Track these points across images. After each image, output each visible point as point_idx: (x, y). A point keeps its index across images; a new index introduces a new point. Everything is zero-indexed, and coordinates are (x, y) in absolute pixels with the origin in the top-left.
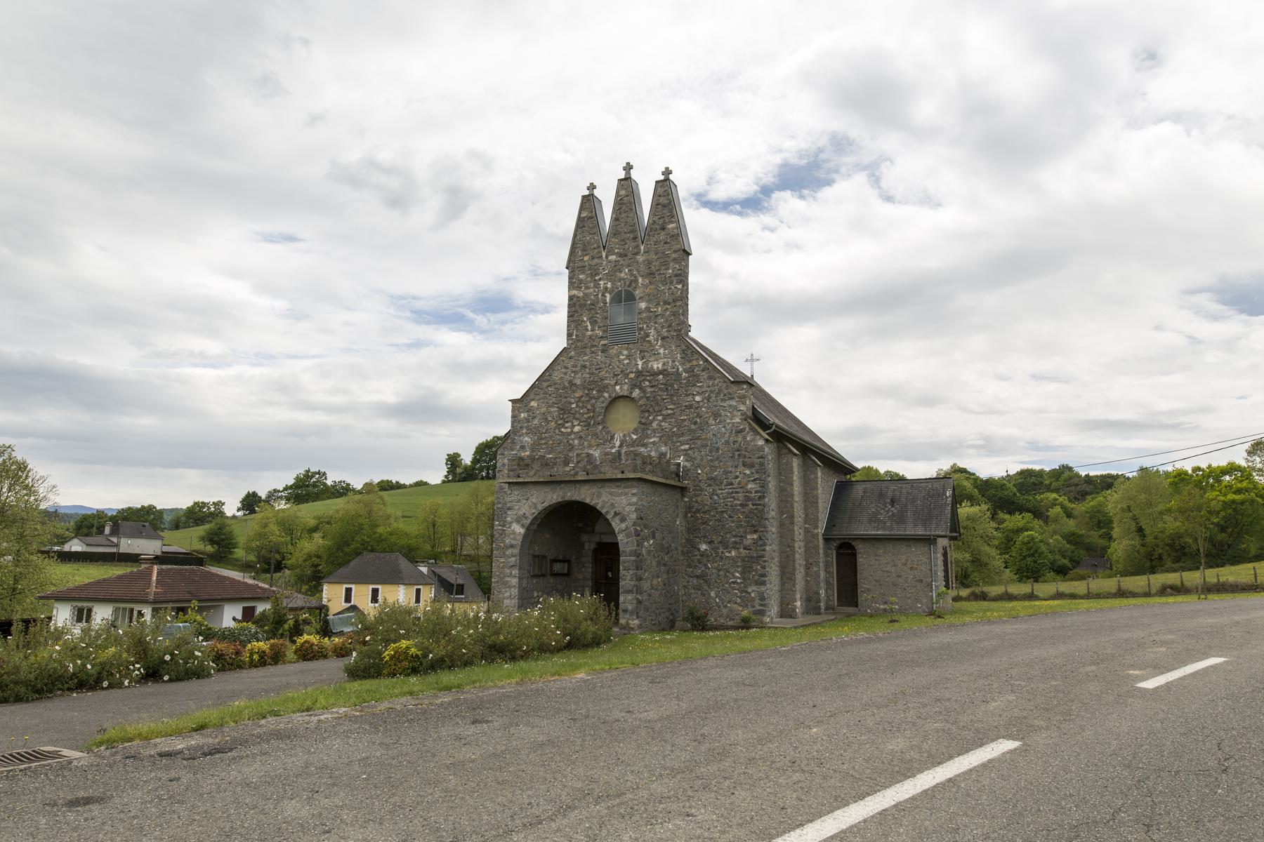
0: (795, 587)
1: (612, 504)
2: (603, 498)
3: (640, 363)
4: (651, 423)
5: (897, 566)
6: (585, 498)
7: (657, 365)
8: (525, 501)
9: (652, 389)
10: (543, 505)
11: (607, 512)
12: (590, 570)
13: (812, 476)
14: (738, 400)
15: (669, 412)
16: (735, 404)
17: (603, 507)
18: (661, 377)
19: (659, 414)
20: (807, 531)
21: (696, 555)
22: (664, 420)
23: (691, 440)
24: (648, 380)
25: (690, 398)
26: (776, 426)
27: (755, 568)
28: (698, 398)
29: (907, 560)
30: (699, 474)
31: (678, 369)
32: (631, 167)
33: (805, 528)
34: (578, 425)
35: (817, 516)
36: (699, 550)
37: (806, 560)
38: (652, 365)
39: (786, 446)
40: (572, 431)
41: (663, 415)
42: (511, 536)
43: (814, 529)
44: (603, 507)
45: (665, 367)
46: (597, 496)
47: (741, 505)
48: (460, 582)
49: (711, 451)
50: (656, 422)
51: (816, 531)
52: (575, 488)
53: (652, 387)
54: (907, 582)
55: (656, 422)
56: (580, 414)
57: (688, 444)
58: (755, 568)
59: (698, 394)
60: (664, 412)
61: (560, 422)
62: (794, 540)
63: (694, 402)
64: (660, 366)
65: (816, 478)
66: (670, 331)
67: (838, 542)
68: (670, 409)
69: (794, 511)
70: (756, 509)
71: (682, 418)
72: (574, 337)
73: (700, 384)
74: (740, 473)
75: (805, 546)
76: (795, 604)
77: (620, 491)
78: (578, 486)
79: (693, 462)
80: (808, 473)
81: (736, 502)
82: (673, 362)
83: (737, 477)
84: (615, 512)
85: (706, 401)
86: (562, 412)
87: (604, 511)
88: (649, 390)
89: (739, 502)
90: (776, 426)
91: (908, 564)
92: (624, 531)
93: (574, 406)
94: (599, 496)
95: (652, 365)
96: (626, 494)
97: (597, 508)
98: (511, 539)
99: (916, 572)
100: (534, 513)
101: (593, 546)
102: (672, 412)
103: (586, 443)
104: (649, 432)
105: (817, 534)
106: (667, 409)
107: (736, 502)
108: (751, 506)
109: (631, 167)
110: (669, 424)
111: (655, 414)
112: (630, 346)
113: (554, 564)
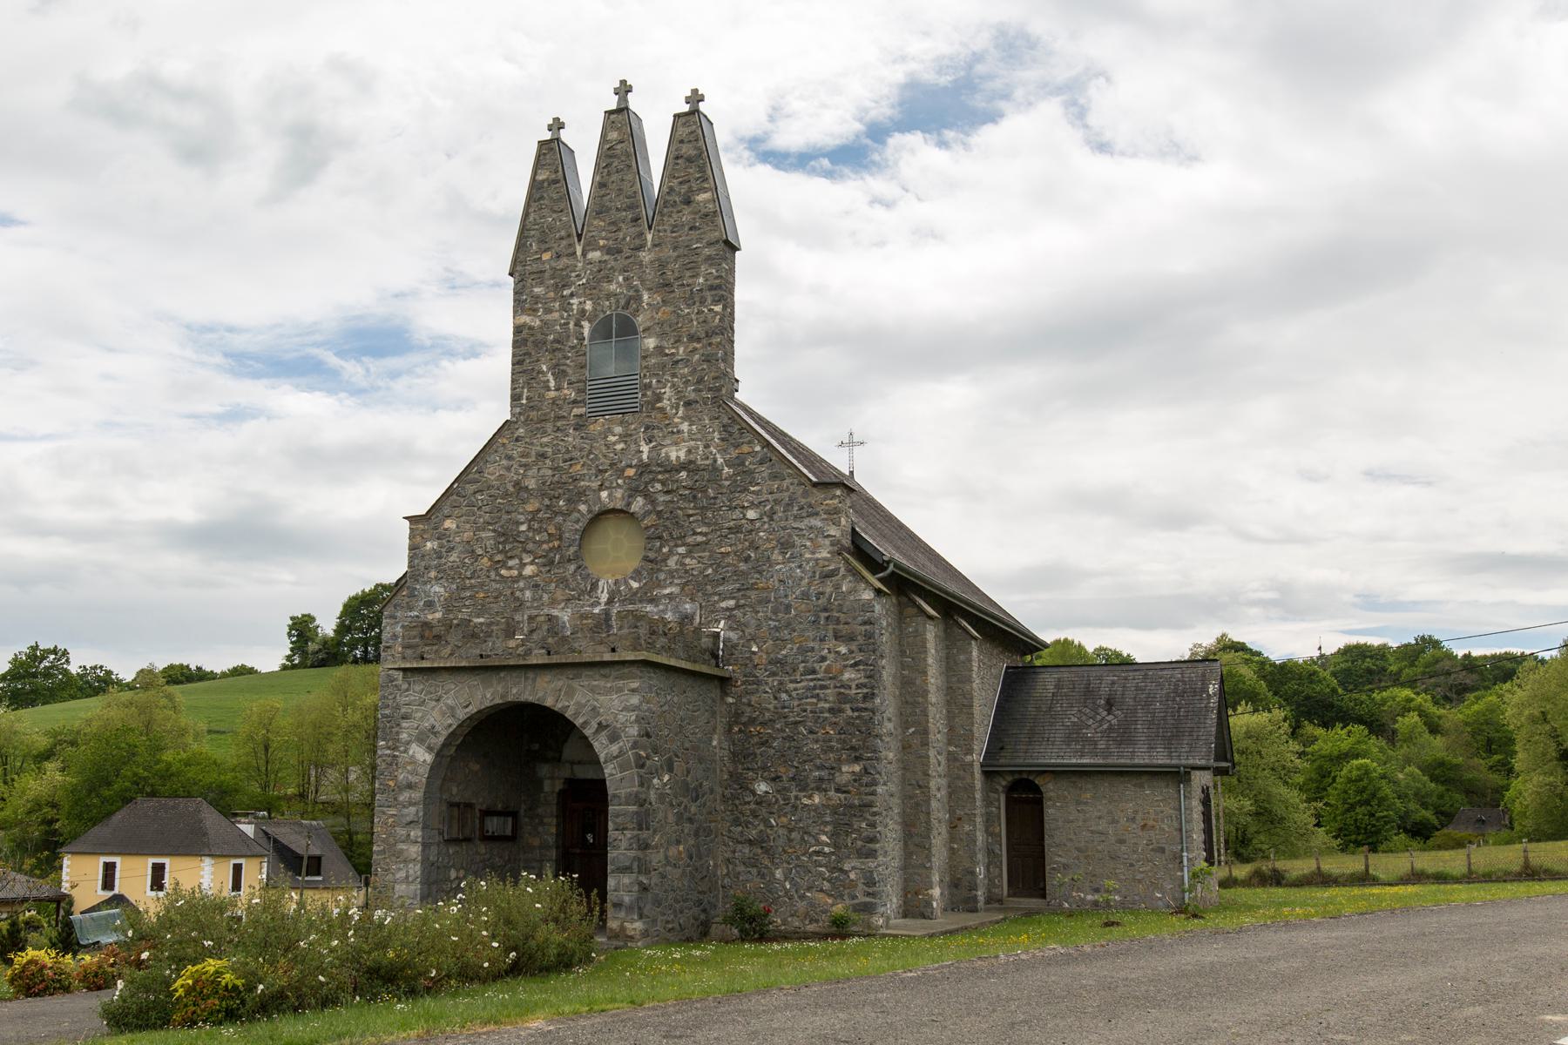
0: (930, 861)
2: (578, 697)
3: (645, 448)
5: (1118, 822)
7: (676, 454)
9: (668, 498)
10: (467, 710)
11: (586, 723)
12: (554, 830)
13: (962, 657)
15: (700, 539)
16: (819, 524)
17: (577, 714)
18: (684, 474)
20: (952, 758)
23: (739, 590)
27: (855, 827)
29: (1136, 812)
30: (754, 653)
31: (715, 461)
35: (971, 731)
36: (754, 793)
38: (666, 453)
39: (914, 602)
40: (520, 575)
43: (966, 754)
44: (577, 714)
45: (692, 457)
47: (831, 710)
50: (676, 558)
51: (969, 758)
52: (526, 678)
53: (668, 492)
54: (1135, 852)
55: (676, 558)
58: (855, 827)
59: (753, 505)
60: (690, 540)
61: (499, 557)
62: (928, 775)
64: (682, 454)
65: (970, 660)
67: (1010, 778)
68: (700, 533)
70: (858, 718)
72: (524, 401)
75: (949, 787)
76: (930, 892)
78: (531, 675)
79: (743, 631)
80: (955, 651)
82: (707, 446)
83: (823, 659)
84: (600, 724)
87: (578, 722)
89: (827, 706)
93: (523, 528)
94: (570, 693)
96: (620, 690)
99: (1152, 833)
101: (559, 786)
102: (704, 539)
103: (546, 596)
104: (662, 576)
105: (971, 764)
106: (695, 533)
107: (821, 704)
109: (629, 90)
110: (699, 562)
111: (672, 544)
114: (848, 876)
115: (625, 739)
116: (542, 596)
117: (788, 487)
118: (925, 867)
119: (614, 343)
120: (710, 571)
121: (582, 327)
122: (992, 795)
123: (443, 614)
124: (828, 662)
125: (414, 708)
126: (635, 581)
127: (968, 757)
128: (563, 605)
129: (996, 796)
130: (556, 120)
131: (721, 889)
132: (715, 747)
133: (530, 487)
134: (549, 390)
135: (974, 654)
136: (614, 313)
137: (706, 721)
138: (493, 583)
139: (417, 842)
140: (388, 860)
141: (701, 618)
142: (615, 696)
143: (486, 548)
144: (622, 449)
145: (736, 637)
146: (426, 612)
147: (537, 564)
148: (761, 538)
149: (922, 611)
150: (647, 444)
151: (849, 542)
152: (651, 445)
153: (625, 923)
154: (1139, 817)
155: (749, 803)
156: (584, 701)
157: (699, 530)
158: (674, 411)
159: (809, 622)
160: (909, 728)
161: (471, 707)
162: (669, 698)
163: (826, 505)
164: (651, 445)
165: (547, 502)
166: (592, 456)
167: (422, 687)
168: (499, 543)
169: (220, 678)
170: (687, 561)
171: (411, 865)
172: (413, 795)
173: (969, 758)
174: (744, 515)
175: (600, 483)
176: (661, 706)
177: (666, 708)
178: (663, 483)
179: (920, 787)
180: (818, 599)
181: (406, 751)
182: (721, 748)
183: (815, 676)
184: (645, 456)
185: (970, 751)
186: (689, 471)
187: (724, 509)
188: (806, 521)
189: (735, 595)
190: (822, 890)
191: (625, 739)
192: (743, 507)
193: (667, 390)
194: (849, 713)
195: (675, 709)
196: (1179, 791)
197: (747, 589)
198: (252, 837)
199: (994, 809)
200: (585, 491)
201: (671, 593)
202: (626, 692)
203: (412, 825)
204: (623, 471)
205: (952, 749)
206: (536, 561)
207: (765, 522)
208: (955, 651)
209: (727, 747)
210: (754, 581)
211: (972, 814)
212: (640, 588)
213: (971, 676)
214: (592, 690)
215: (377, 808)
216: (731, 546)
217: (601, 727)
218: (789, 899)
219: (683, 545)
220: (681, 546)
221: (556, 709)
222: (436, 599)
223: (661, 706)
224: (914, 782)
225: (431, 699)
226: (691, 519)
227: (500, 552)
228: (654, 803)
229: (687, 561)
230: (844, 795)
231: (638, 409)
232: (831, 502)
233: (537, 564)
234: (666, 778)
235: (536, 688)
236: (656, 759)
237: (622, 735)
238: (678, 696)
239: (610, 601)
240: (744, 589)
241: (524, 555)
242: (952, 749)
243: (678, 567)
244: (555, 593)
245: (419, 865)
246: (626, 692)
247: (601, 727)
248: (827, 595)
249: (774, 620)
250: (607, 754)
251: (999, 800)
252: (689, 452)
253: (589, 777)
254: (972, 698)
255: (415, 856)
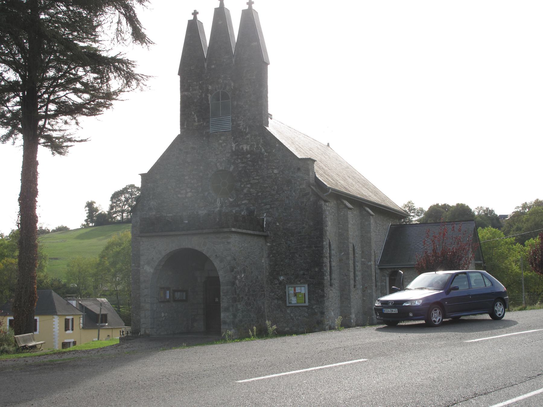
0: (350, 304)
3: (234, 145)
7: (246, 147)
9: (243, 165)
13: (367, 223)
18: (249, 156)
19: (248, 183)
20: (363, 264)
21: (276, 284)
23: (271, 201)
26: (332, 190)
27: (317, 292)
28: (276, 171)
31: (261, 150)
33: (362, 261)
34: (190, 192)
35: (371, 252)
36: (278, 280)
37: (362, 285)
38: (242, 147)
39: (343, 203)
41: (251, 184)
43: (369, 262)
48: (104, 312)
50: (247, 189)
51: (370, 263)
53: (243, 163)
55: (247, 189)
57: (269, 204)
58: (317, 292)
60: (252, 182)
62: (349, 271)
63: (273, 174)
65: (370, 224)
67: (390, 271)
68: (256, 179)
69: (349, 250)
75: (362, 275)
76: (350, 316)
79: (273, 217)
80: (364, 220)
82: (257, 144)
85: (281, 173)
88: (241, 165)
90: (332, 190)
93: (187, 178)
95: (242, 147)
97: (204, 253)
98: (538, 251)
102: (258, 181)
105: (371, 266)
106: (254, 179)
113: (176, 293)
114: (314, 311)
115: (226, 261)
118: (348, 307)
122: (383, 278)
125: (145, 251)
126: (231, 198)
127: (369, 263)
128: (203, 208)
129: (385, 278)
130: (195, 11)
131: (267, 317)
132: (263, 263)
133: (189, 161)
134: (195, 121)
135: (371, 221)
136: (220, 91)
137: (259, 253)
141: (257, 213)
145: (271, 219)
149: (346, 207)
150: (235, 144)
151: (314, 182)
158: (245, 130)
160: (342, 253)
162: (243, 245)
164: (236, 144)
165: (195, 167)
166: (213, 149)
169: (51, 233)
173: (370, 263)
176: (240, 248)
177: (242, 249)
179: (346, 276)
181: (143, 268)
182: (265, 263)
185: (370, 260)
194: (314, 248)
195: (246, 249)
198: (75, 306)
199: (384, 283)
201: (245, 203)
205: (363, 260)
206: (192, 191)
208: (364, 220)
209: (268, 263)
211: (371, 285)
212: (233, 201)
213: (370, 231)
220: (249, 184)
223: (240, 248)
224: (344, 274)
228: (238, 285)
229: (252, 190)
230: (313, 280)
234: (243, 275)
236: (239, 268)
238: (247, 244)
239: (222, 207)
242: (363, 260)
243: (248, 192)
251: (386, 280)
254: (371, 239)
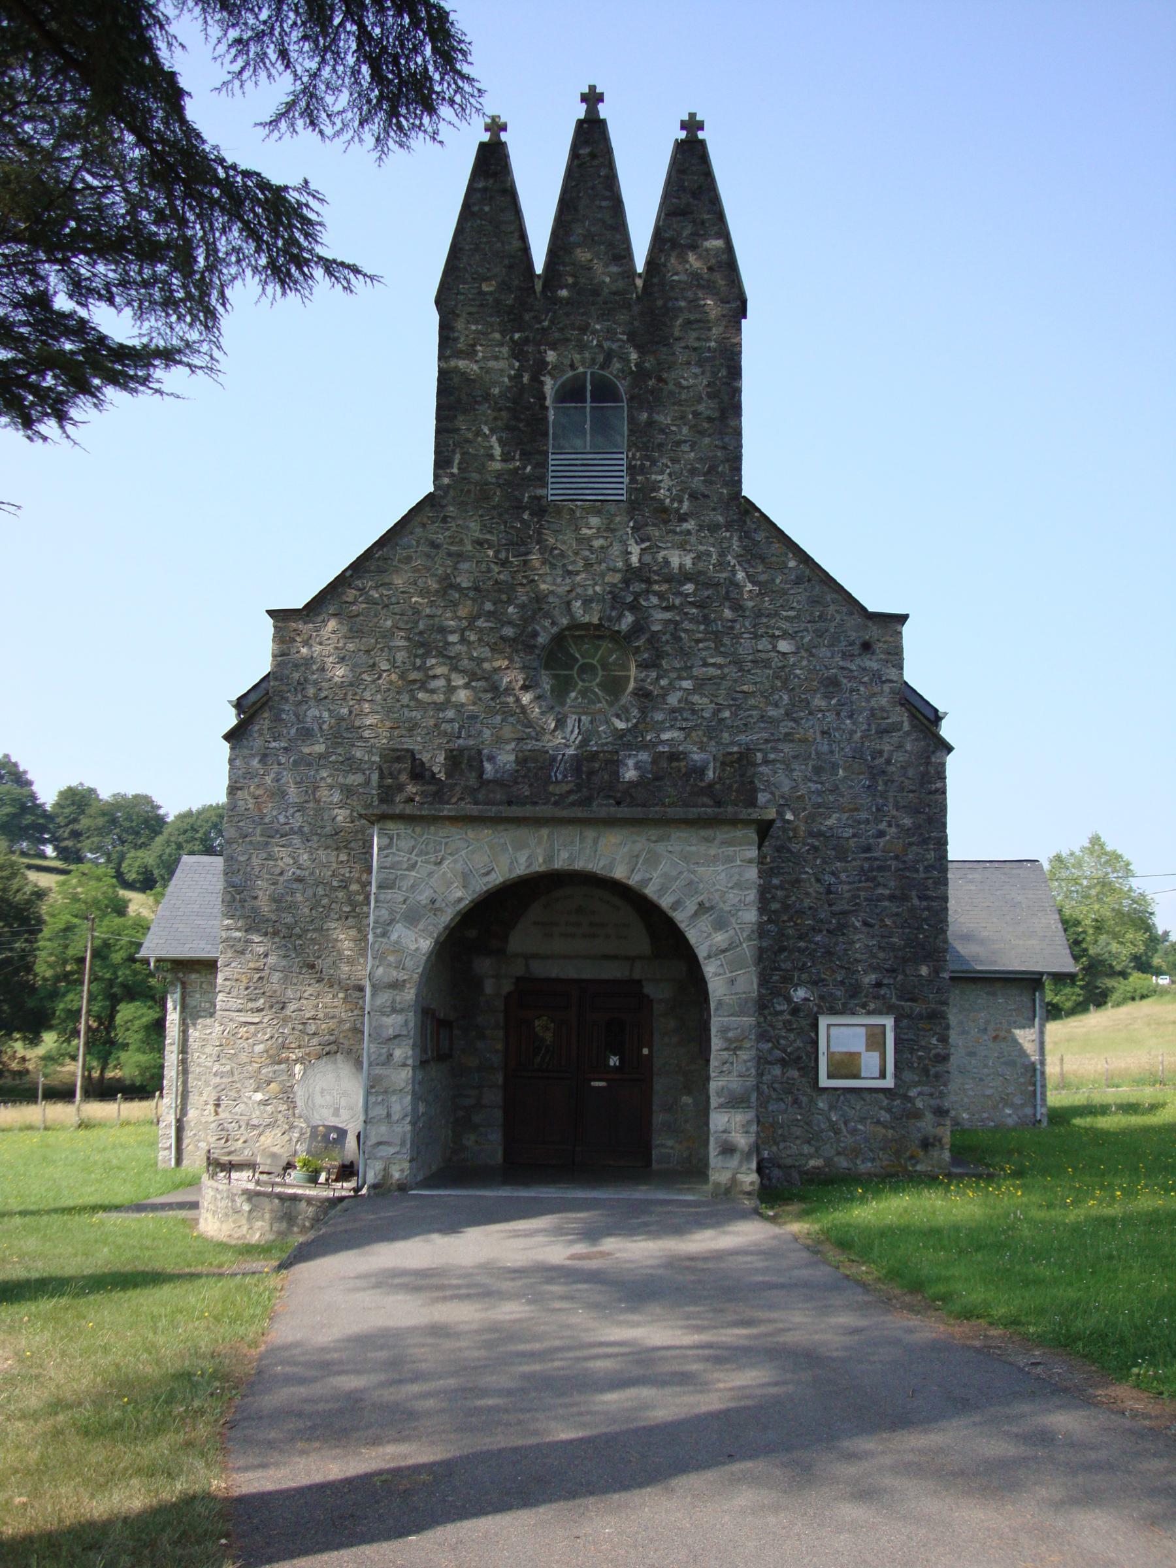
1: (691, 883)
2: (664, 867)
3: (635, 549)
4: (664, 696)
5: (968, 1033)
6: (612, 865)
8: (432, 867)
9: (668, 615)
10: (486, 879)
11: (676, 905)
12: (500, 1046)
14: (883, 656)
15: (712, 671)
16: (875, 665)
17: (663, 890)
18: (689, 588)
22: (698, 688)
23: (767, 741)
24: (656, 593)
25: (764, 644)
28: (784, 646)
29: (987, 1022)
30: (789, 822)
32: (600, 98)
36: (789, 999)
40: (448, 701)
42: (391, 958)
44: (663, 890)
45: (701, 566)
46: (646, 861)
47: (892, 898)
49: (818, 770)
50: (679, 694)
52: (582, 840)
53: (667, 609)
54: (986, 1066)
55: (679, 694)
56: (472, 659)
59: (785, 635)
61: (414, 675)
64: (688, 561)
66: (711, 483)
68: (714, 665)
70: (928, 908)
71: (745, 688)
72: (455, 471)
73: (792, 613)
74: (890, 826)
77: (712, 852)
78: (590, 834)
79: (772, 793)
81: (880, 891)
82: (722, 554)
83: (881, 834)
84: (701, 904)
86: (421, 651)
87: (665, 903)
89: (887, 892)
91: (990, 1028)
92: (724, 951)
94: (653, 860)
96: (729, 860)
99: (1003, 1045)
100: (460, 900)
101: (507, 987)
102: (719, 672)
103: (487, 733)
104: (659, 716)
107: (880, 891)
108: (916, 902)
109: (600, 98)
110: (712, 702)
111: (673, 675)
112: (607, 506)
115: (737, 927)
116: (481, 731)
117: (833, 616)
119: (588, 410)
120: (727, 714)
121: (542, 383)
123: (327, 748)
124: (888, 838)
138: (406, 711)
139: (404, 1065)
140: (238, 1085)
142: (721, 868)
143: (395, 661)
144: (602, 547)
146: (299, 743)
147: (474, 688)
148: (797, 676)
152: (643, 546)
153: (739, 1176)
154: (990, 1027)
155: (782, 1012)
156: (674, 873)
157: (711, 661)
159: (863, 787)
161: (493, 876)
163: (885, 642)
164: (643, 546)
167: (413, 842)
168: (416, 656)
170: (696, 698)
171: (394, 1098)
172: (398, 998)
174: (775, 647)
175: (568, 588)
178: (661, 596)
180: (873, 759)
183: (868, 855)
184: (634, 560)
186: (697, 584)
187: (746, 636)
188: (858, 661)
189: (763, 747)
190: (878, 1122)
191: (737, 927)
192: (773, 636)
193: (665, 477)
196: (1034, 1001)
197: (779, 740)
200: (546, 596)
201: (672, 739)
202: (739, 863)
203: (396, 1041)
204: (603, 575)
206: (473, 684)
207: (802, 657)
210: (787, 730)
214: (686, 858)
215: (219, 1013)
216: (755, 683)
217: (703, 909)
218: (836, 1133)
219: (690, 678)
221: (631, 882)
222: (316, 727)
225: (427, 862)
226: (701, 645)
227: (419, 669)
229: (696, 698)
231: (624, 498)
232: (891, 639)
233: (474, 688)
235: (598, 853)
237: (733, 921)
240: (774, 741)
241: (453, 676)
244: (501, 729)
245: (409, 1097)
246: (739, 863)
247: (702, 908)
248: (886, 755)
249: (816, 782)
250: (710, 946)
252: (698, 557)
253: (554, 975)
255: (403, 1085)
